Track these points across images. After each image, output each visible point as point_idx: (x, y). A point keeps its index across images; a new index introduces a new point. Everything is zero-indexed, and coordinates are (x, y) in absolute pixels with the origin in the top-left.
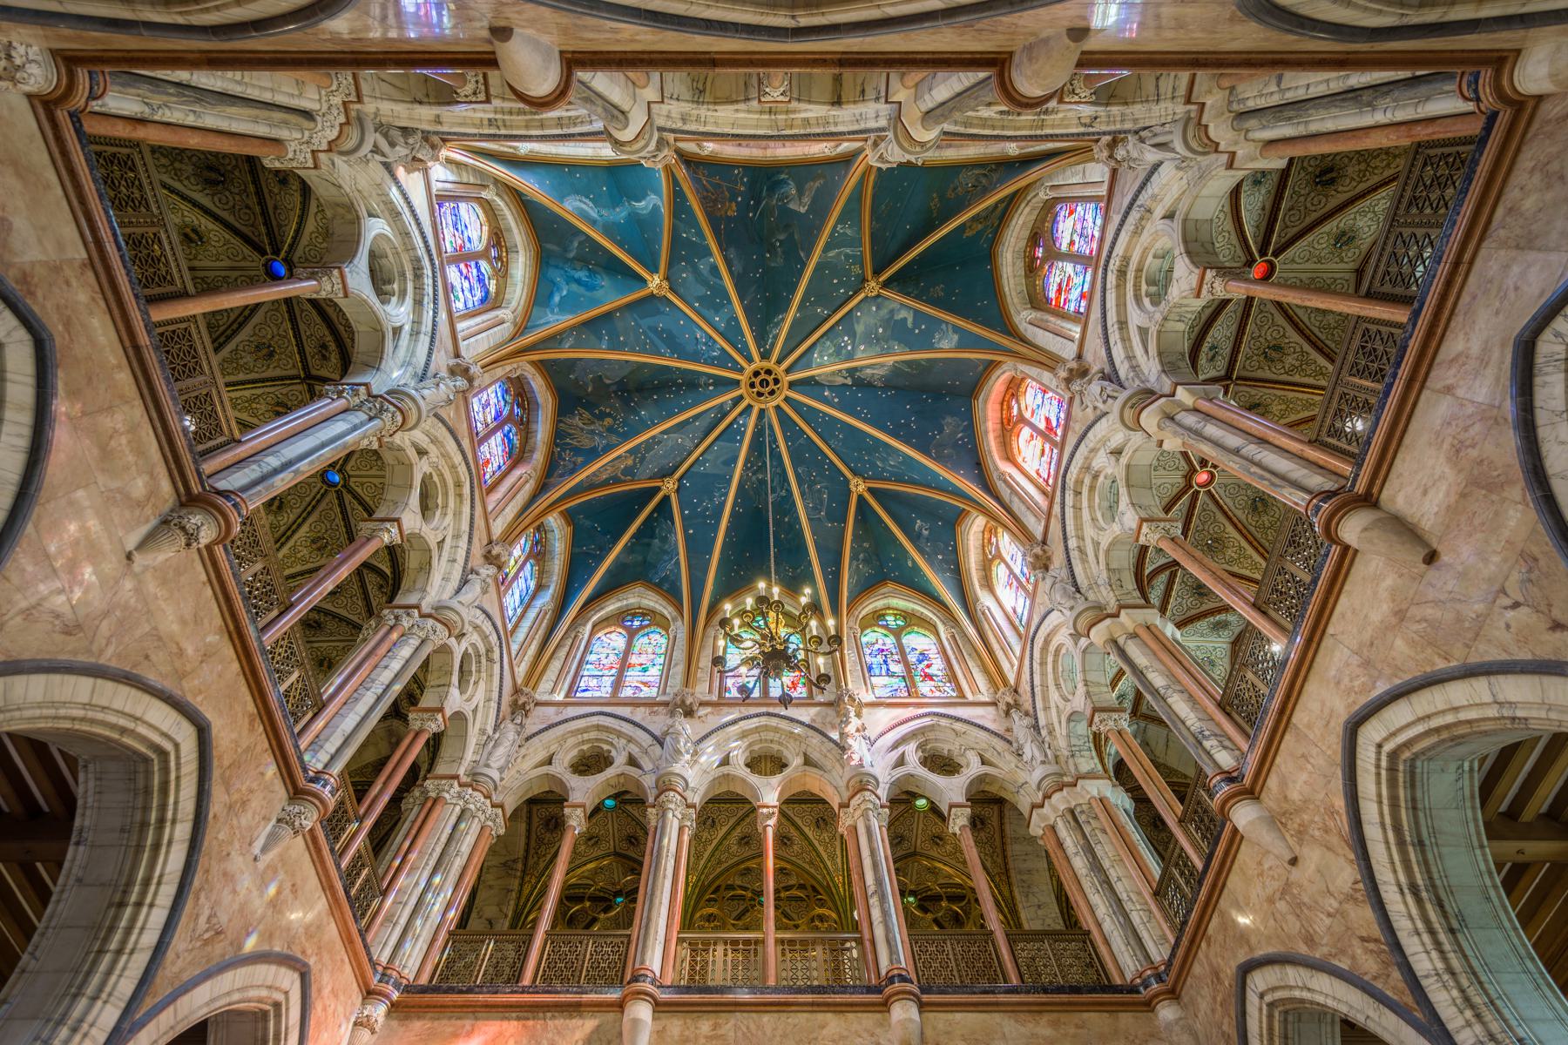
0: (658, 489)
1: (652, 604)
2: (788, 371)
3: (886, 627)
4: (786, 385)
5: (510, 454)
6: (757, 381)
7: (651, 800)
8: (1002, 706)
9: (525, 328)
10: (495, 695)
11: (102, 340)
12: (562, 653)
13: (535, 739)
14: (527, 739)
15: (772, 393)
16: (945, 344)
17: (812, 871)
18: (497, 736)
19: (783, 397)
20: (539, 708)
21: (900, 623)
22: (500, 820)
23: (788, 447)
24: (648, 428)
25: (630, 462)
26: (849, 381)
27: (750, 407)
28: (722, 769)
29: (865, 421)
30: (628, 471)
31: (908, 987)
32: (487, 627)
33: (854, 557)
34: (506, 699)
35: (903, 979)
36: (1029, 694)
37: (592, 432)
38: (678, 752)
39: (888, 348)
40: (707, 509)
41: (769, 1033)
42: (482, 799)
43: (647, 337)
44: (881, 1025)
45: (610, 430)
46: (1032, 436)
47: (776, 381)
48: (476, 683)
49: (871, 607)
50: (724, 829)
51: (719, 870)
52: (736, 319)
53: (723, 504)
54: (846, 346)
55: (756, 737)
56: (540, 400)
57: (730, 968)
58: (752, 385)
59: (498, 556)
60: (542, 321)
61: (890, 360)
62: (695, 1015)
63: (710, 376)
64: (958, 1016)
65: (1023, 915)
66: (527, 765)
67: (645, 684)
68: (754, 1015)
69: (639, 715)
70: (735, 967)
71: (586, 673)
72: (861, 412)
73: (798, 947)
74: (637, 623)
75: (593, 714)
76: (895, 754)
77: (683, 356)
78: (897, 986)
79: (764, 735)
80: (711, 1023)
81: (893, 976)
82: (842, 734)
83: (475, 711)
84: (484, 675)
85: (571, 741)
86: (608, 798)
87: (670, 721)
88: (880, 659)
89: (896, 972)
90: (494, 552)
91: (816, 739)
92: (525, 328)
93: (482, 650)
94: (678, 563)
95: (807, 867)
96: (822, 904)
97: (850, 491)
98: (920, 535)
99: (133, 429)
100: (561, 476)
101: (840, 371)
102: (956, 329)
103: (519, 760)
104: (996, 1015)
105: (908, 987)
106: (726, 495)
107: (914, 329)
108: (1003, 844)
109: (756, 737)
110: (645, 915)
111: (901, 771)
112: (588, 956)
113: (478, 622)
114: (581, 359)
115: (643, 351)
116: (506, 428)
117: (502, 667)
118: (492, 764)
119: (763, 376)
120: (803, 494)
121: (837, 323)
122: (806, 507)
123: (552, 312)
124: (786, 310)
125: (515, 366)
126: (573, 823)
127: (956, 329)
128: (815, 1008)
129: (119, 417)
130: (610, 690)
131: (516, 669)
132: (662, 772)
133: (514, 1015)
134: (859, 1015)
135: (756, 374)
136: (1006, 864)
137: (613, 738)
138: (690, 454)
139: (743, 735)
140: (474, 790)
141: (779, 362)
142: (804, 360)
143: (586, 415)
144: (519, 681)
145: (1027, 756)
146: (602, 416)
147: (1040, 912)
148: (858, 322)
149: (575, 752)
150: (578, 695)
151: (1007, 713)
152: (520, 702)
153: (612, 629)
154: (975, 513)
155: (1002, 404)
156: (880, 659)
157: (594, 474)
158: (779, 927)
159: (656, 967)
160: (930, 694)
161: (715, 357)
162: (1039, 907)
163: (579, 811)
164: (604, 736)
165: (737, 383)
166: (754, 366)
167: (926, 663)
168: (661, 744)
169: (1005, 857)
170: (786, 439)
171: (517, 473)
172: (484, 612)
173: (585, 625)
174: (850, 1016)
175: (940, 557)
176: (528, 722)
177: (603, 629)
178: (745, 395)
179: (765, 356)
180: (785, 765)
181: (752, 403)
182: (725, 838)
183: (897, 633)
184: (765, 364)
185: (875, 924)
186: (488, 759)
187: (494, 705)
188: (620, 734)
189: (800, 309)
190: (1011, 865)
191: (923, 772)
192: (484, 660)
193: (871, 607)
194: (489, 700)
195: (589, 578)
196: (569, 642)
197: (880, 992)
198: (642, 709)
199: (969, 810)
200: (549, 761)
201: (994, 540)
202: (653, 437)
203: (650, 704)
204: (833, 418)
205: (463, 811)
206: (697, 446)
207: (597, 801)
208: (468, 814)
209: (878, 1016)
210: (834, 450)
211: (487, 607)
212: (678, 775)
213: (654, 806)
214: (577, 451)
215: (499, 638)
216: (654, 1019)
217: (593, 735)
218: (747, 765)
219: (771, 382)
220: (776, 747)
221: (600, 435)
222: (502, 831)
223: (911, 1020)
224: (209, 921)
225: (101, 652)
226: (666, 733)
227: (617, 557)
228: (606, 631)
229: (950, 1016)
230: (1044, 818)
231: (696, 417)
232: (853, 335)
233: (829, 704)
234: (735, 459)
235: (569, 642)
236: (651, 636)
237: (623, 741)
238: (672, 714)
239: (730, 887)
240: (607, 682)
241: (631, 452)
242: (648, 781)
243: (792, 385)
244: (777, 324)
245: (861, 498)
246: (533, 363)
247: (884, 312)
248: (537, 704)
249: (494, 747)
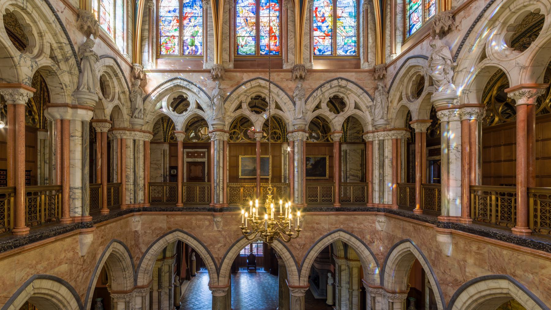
11: (180, 219)
13: (391, 90)
14: (388, 92)
41: (506, 260)
42: (383, 132)
46: (174, 11)
99: (196, 219)
129: (193, 222)
139: (492, 22)
140: (378, 132)
224: (299, 245)
225: (232, 242)
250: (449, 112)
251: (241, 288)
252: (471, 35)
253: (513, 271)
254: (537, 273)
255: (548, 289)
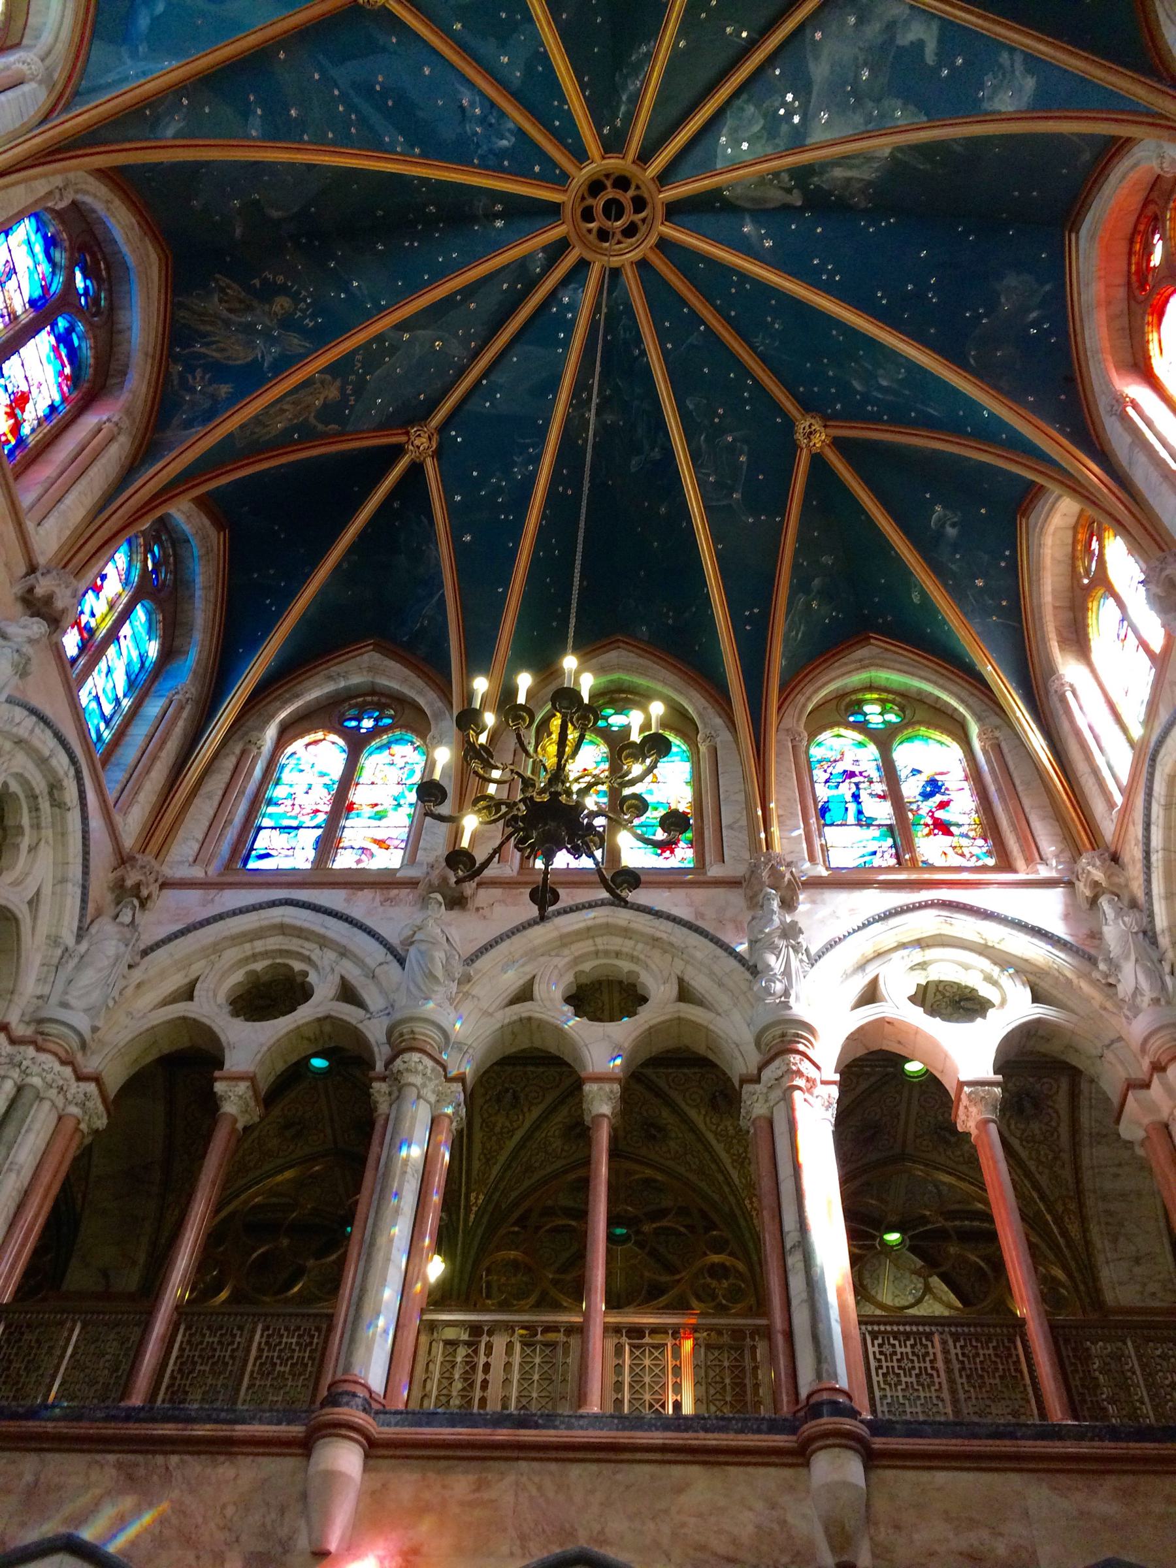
0: (397, 451)
1: (395, 685)
2: (664, 178)
3: (862, 727)
4: (660, 212)
5: (74, 380)
6: (599, 203)
7: (379, 1066)
8: (1084, 890)
9: (76, 93)
10: (76, 871)
12: (216, 784)
13: (161, 953)
14: (145, 953)
15: (630, 231)
16: (1005, 102)
17: (703, 1185)
18: (83, 947)
19: (653, 240)
20: (168, 893)
21: (892, 718)
22: (97, 1105)
23: (665, 354)
24: (367, 317)
25: (333, 393)
26: (796, 199)
27: (583, 265)
28: (517, 1008)
29: (828, 289)
30: (330, 412)
31: (848, 1424)
32: (45, 742)
33: (801, 585)
34: (101, 878)
35: (838, 1410)
36: (1139, 866)
37: (248, 329)
38: (431, 976)
39: (882, 116)
40: (499, 491)
42: (57, 1067)
43: (351, 107)
44: (792, 1489)
45: (287, 323)
47: (640, 204)
48: (32, 849)
49: (832, 687)
50: (536, 1112)
51: (527, 1183)
52: (545, 58)
53: (532, 479)
54: (789, 115)
55: (585, 946)
56: (131, 260)
57: (516, 1376)
58: (588, 215)
59: (49, 599)
60: (110, 78)
61: (883, 145)
62: (443, 1464)
63: (496, 196)
64: (941, 1477)
65: (1107, 1274)
66: (152, 997)
67: (380, 843)
68: (553, 1467)
69: (361, 905)
70: (525, 1377)
71: (266, 822)
72: (820, 269)
73: (647, 1340)
74: (367, 723)
75: (273, 904)
76: (859, 983)
77: (434, 150)
78: (827, 1422)
79: (602, 943)
80: (472, 1478)
81: (820, 1404)
82: (753, 943)
83: (34, 903)
84: (48, 833)
85: (232, 954)
86: (316, 1055)
87: (418, 917)
88: (846, 790)
89: (825, 1396)
90: (40, 591)
91: (700, 948)
92: (76, 93)
93: (40, 785)
94: (442, 602)
95: (693, 1177)
96: (718, 1246)
97: (795, 447)
98: (940, 534)
100: (188, 424)
101: (776, 174)
102: (1033, 63)
103: (129, 991)
104: (1014, 1477)
105: (848, 1424)
106: (537, 460)
107: (939, 67)
108: (1075, 1145)
109: (585, 946)
110: (357, 1283)
111: (869, 1013)
112: (254, 1352)
113: (23, 732)
114: (207, 164)
115: (344, 141)
116: (62, 324)
117: (85, 819)
118: (73, 1002)
119: (610, 193)
120: (695, 457)
121: (770, 61)
122: (702, 484)
123: (134, 55)
124: (653, 32)
125: (58, 181)
126: (230, 1108)
127: (1033, 63)
128: (669, 1456)
130: (311, 854)
131: (118, 818)
132: (398, 1016)
133: (111, 1458)
134: (750, 1470)
135: (595, 187)
136: (1078, 1181)
137: (310, 949)
138: (462, 372)
140: (39, 1049)
141: (644, 157)
142: (698, 153)
143: (234, 290)
144: (129, 841)
145: (1125, 987)
146: (268, 293)
147: (1137, 1270)
148: (817, 58)
149: (238, 976)
150: (252, 865)
151: (1093, 902)
152: (129, 883)
153: (320, 735)
154: (1054, 489)
155: (1131, 242)
156: (846, 790)
157: (257, 420)
158: (614, 1302)
159: (376, 1378)
160: (939, 862)
161: (503, 153)
162: (1137, 1261)
163: (242, 1087)
164: (294, 944)
165: (553, 210)
166: (589, 170)
167: (938, 798)
168: (401, 961)
169: (1077, 1169)
170: (662, 336)
171: (90, 421)
172: (33, 711)
173: (262, 728)
174: (733, 1470)
175: (980, 583)
176: (143, 919)
177: (301, 735)
178: (573, 239)
179: (613, 144)
180: (644, 1000)
181: (588, 256)
182: (536, 1126)
183: (884, 740)
184: (613, 163)
185: (795, 1302)
186: (65, 993)
187: (74, 891)
188: (323, 942)
189: (682, 32)
190: (1088, 1183)
191: (916, 1017)
192: (45, 805)
193: (832, 687)
194: (63, 880)
195: (263, 638)
196: (229, 763)
197: (793, 1430)
198: (367, 894)
199: (998, 1090)
200: (188, 993)
201: (1095, 545)
202: (380, 338)
203: (384, 882)
204: (759, 284)
205: (20, 1089)
206: (476, 355)
207: (294, 1058)
208: (28, 1095)
209: (787, 1473)
210: (763, 358)
211: (36, 702)
212: (426, 1020)
213: (384, 1079)
214: (219, 371)
215: (73, 760)
216: (366, 1469)
217: (274, 942)
218: (569, 1000)
219: (629, 206)
220: (625, 966)
221: (266, 334)
222: (101, 1123)
223: (846, 1485)
226: (409, 942)
227: (322, 592)
228: (308, 739)
229: (925, 1476)
230: (1152, 1108)
231: (469, 291)
232: (803, 88)
233: (732, 883)
234: (553, 384)
235: (229, 763)
236: (395, 748)
237: (330, 955)
238: (424, 902)
239: (548, 1212)
240: (308, 838)
241: (334, 370)
242: (375, 1031)
243: (673, 211)
244: (637, 68)
245: (818, 462)
246: (102, 174)
247: (873, 30)
248: (165, 885)
249: (78, 968)
250: (433, 1070)
251: (174, 1048)
252: (515, 939)
253: (597, 1527)
254: (666, 1511)
255: (695, 1549)
